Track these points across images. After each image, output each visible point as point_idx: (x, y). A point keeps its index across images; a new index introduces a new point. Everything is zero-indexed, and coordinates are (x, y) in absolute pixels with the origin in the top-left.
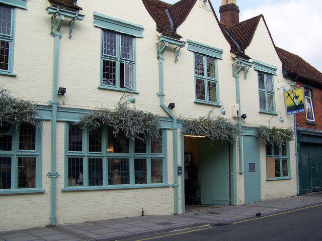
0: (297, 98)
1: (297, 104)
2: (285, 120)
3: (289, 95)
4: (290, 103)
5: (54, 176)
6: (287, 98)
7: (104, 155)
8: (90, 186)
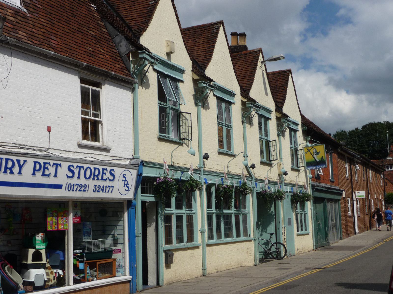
0: (318, 154)
1: (318, 160)
2: (302, 174)
3: (309, 151)
4: (311, 159)
5: (203, 232)
6: (306, 153)
7: (299, 212)
8: (226, 239)
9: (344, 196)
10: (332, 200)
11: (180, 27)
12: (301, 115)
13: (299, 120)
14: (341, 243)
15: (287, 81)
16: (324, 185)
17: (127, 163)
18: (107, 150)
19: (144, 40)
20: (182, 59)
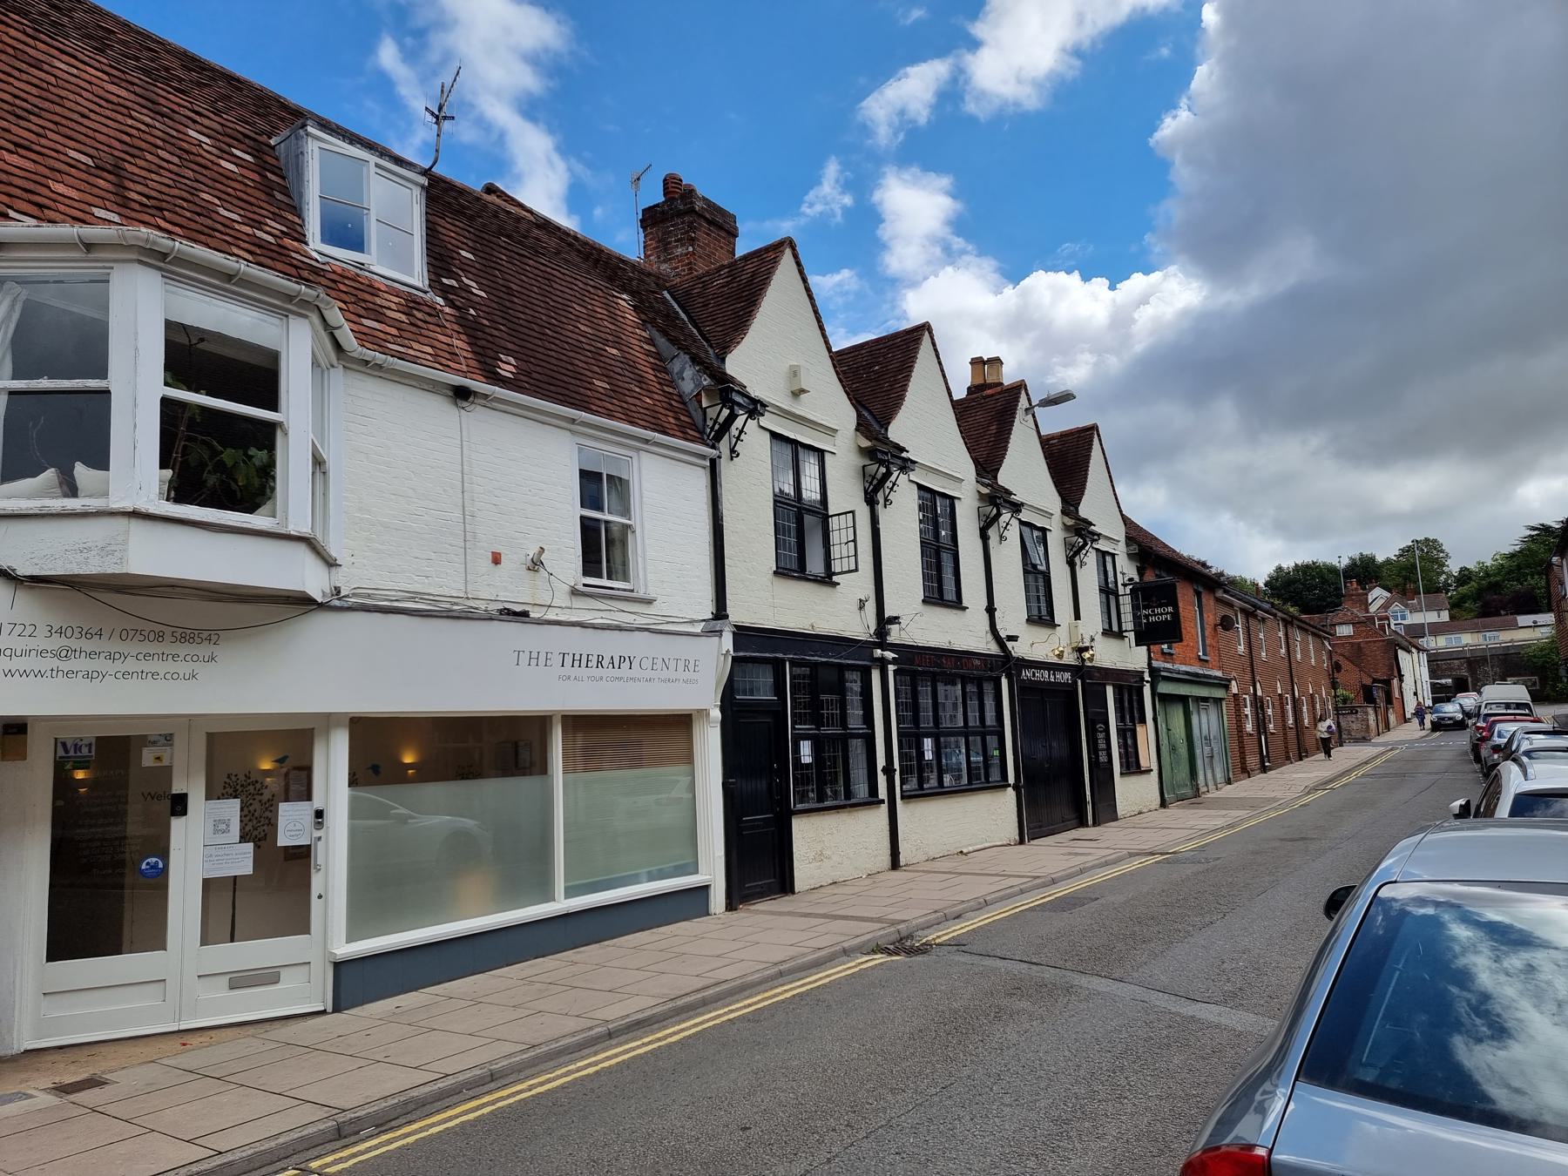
9: (1235, 690)
10: (1205, 699)
11: (829, 349)
12: (1125, 520)
13: (1119, 533)
14: (1228, 791)
15: (1090, 449)
16: (1184, 668)
17: (698, 629)
18: (649, 602)
19: (737, 364)
20: (833, 410)
